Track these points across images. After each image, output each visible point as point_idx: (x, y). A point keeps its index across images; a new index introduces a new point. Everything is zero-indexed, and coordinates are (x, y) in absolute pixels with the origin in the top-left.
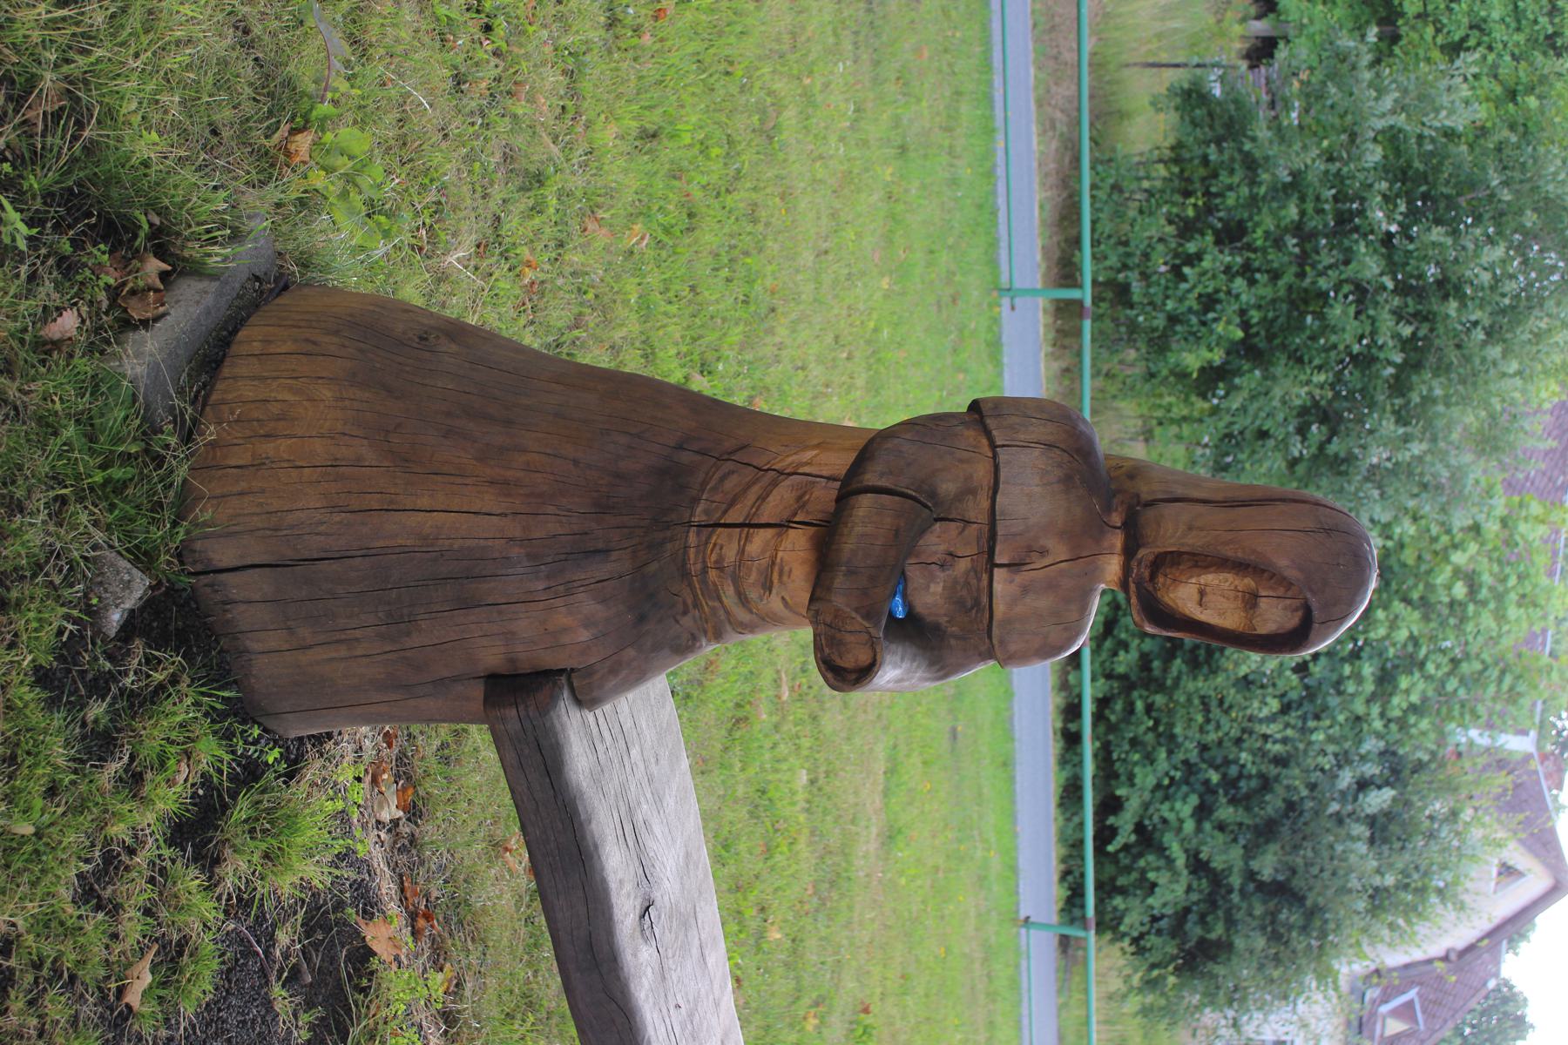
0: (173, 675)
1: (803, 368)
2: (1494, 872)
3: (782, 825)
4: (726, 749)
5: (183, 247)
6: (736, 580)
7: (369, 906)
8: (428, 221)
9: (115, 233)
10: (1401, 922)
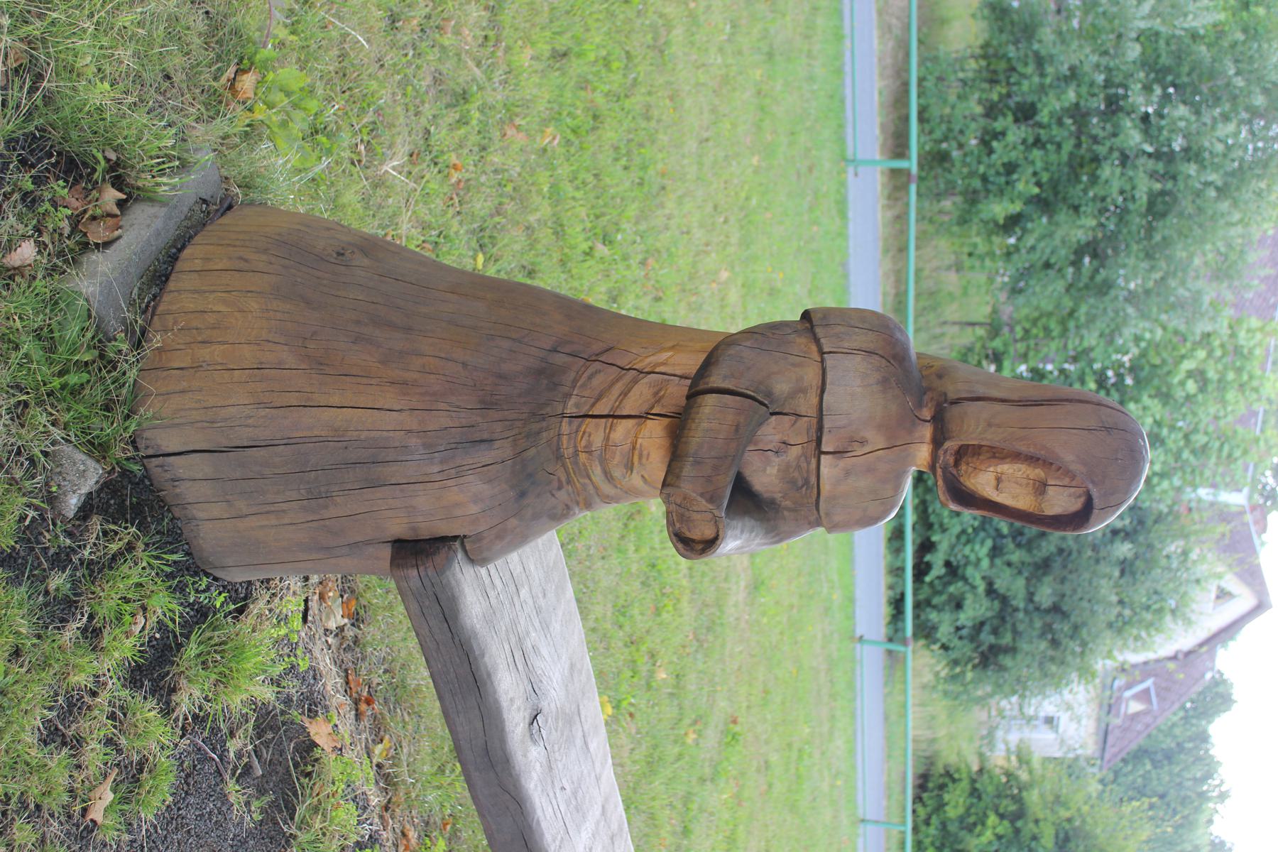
0: (128, 543)
1: (688, 233)
2: (1213, 596)
3: (668, 590)
4: (623, 537)
5: (137, 178)
6: (603, 462)
7: (313, 705)
8: (365, 138)
9: (74, 168)
10: (1143, 634)
